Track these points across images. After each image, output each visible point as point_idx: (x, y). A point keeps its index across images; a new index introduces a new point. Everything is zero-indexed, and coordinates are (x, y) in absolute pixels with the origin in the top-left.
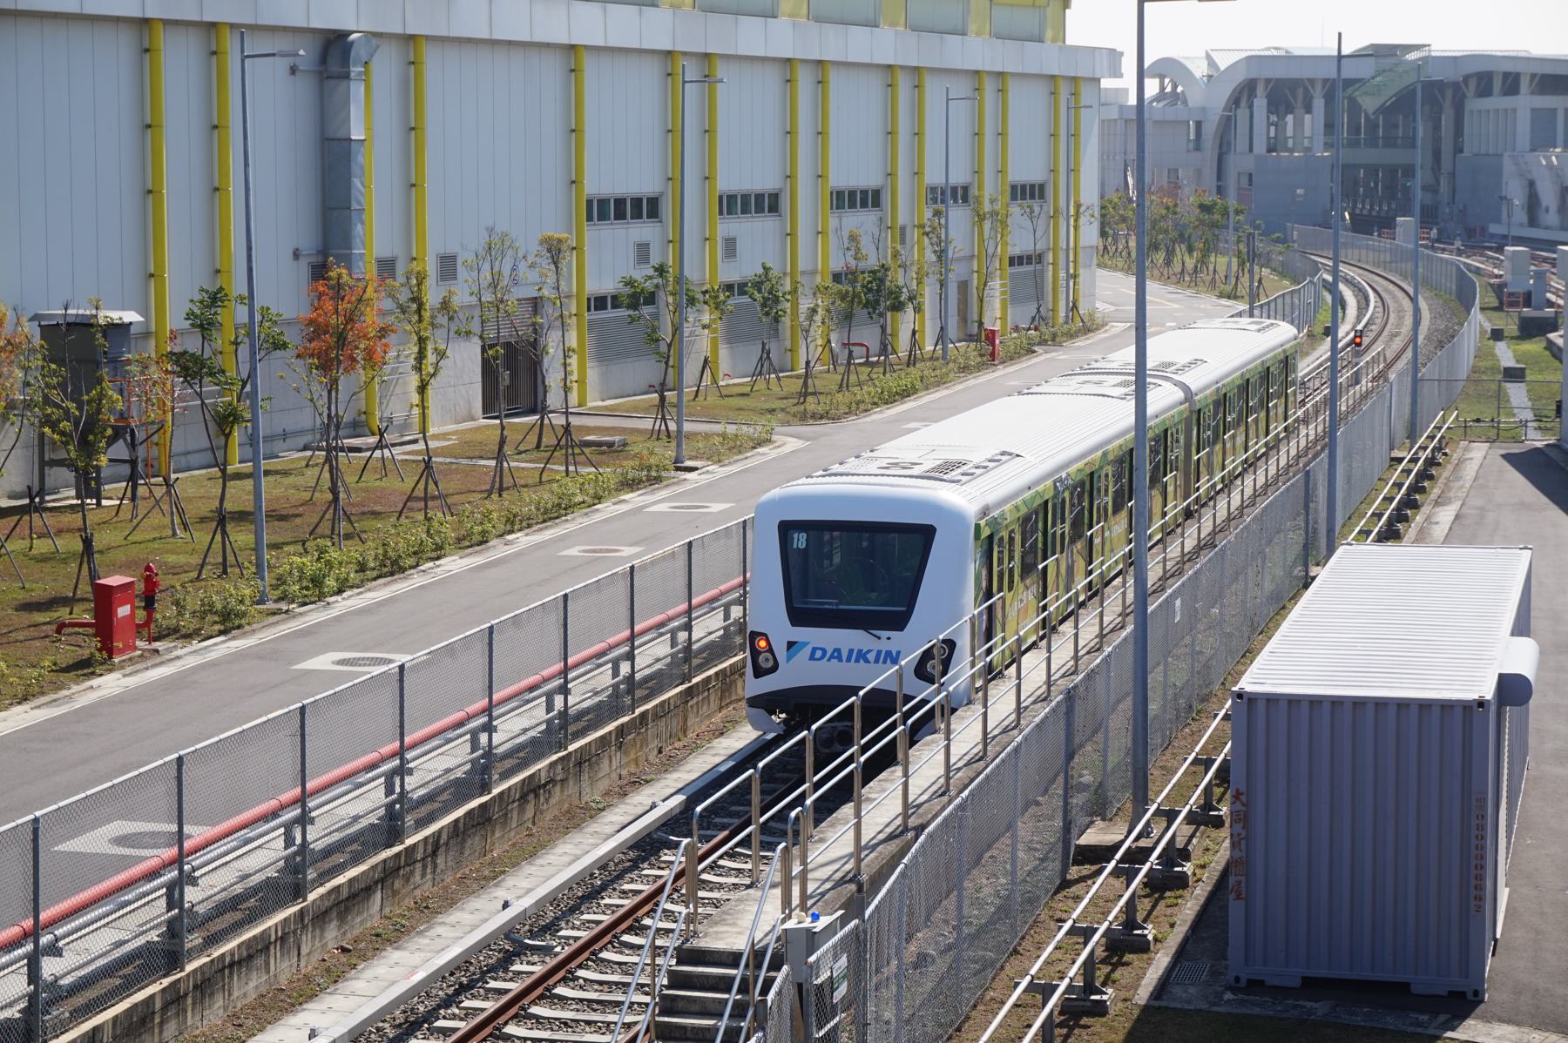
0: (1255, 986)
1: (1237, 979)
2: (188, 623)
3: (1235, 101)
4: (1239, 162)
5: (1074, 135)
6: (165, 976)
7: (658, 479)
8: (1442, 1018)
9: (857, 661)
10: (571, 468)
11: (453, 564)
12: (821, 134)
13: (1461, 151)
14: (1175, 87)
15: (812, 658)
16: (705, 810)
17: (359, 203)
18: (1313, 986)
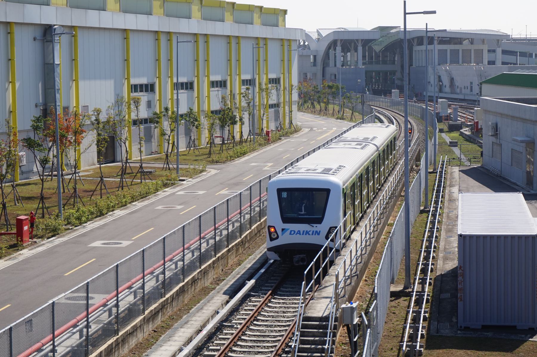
0: (467, 328)
1: (461, 327)
2: (40, 233)
3: (329, 48)
4: (331, 70)
5: (289, 60)
6: (114, 336)
7: (173, 184)
8: (529, 336)
9: (306, 234)
10: (143, 181)
11: (119, 213)
12: (207, 60)
13: (412, 65)
14: (304, 43)
15: (290, 234)
16: (307, 272)
17: (58, 86)
18: (485, 328)
